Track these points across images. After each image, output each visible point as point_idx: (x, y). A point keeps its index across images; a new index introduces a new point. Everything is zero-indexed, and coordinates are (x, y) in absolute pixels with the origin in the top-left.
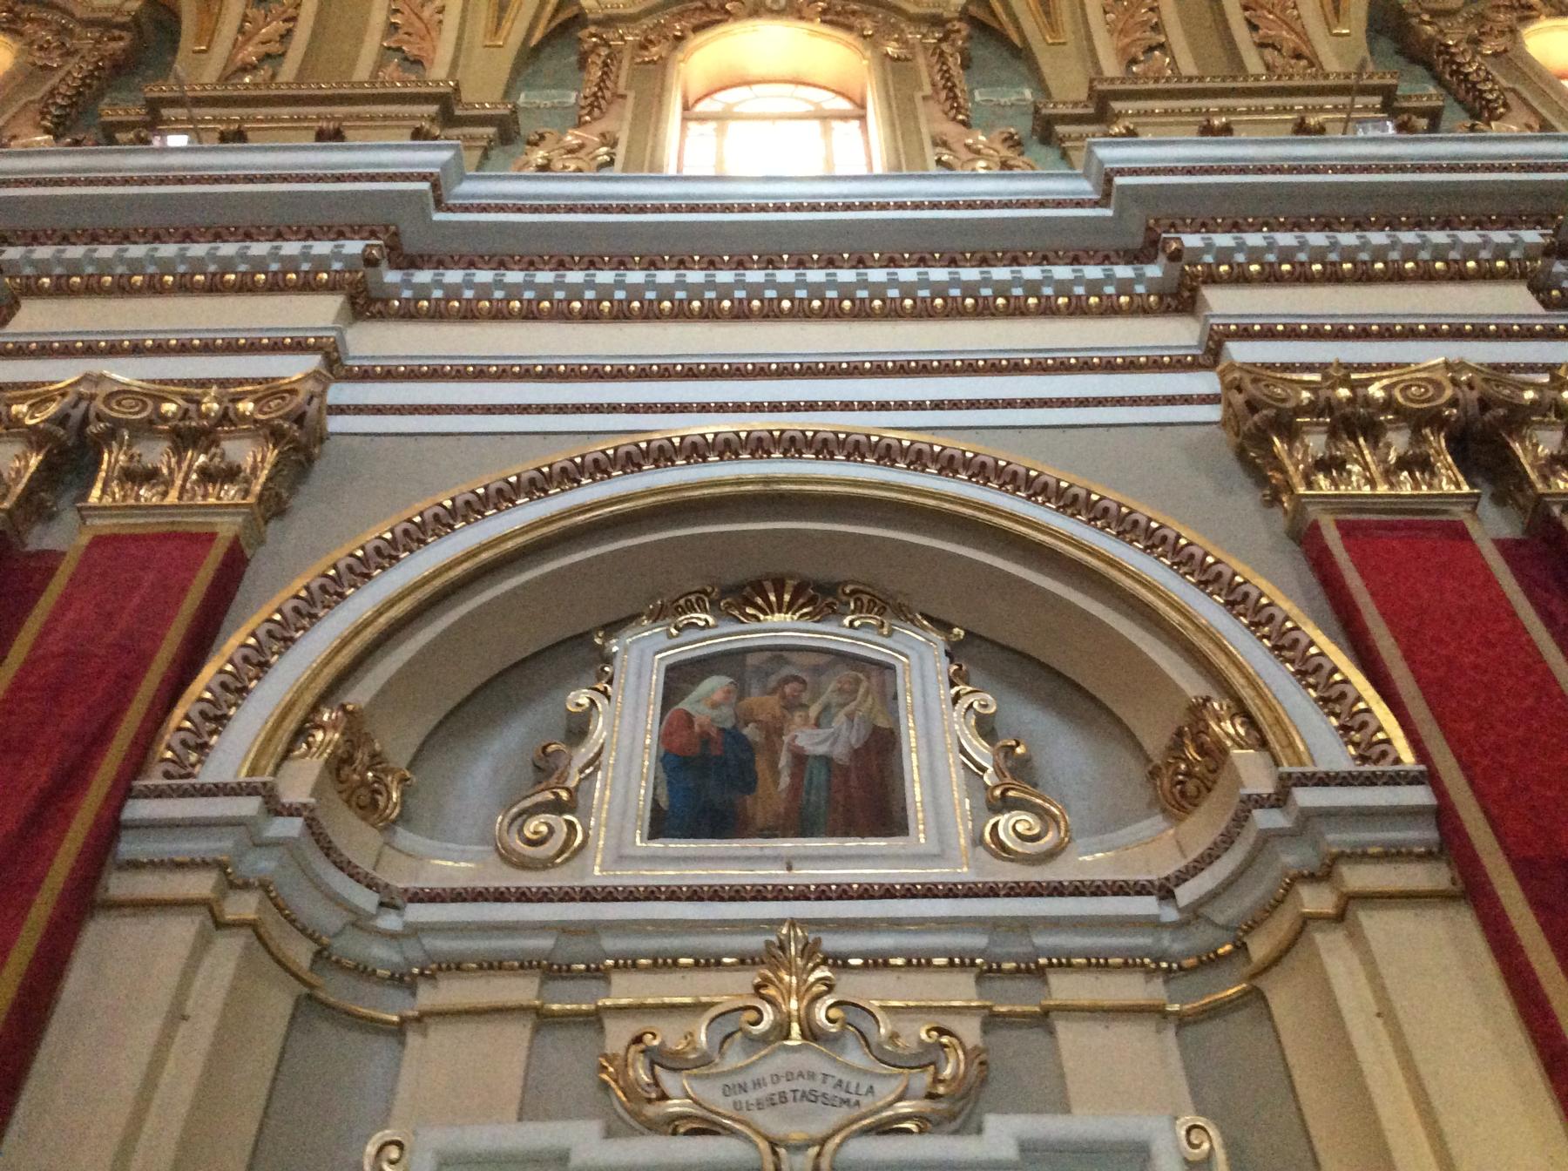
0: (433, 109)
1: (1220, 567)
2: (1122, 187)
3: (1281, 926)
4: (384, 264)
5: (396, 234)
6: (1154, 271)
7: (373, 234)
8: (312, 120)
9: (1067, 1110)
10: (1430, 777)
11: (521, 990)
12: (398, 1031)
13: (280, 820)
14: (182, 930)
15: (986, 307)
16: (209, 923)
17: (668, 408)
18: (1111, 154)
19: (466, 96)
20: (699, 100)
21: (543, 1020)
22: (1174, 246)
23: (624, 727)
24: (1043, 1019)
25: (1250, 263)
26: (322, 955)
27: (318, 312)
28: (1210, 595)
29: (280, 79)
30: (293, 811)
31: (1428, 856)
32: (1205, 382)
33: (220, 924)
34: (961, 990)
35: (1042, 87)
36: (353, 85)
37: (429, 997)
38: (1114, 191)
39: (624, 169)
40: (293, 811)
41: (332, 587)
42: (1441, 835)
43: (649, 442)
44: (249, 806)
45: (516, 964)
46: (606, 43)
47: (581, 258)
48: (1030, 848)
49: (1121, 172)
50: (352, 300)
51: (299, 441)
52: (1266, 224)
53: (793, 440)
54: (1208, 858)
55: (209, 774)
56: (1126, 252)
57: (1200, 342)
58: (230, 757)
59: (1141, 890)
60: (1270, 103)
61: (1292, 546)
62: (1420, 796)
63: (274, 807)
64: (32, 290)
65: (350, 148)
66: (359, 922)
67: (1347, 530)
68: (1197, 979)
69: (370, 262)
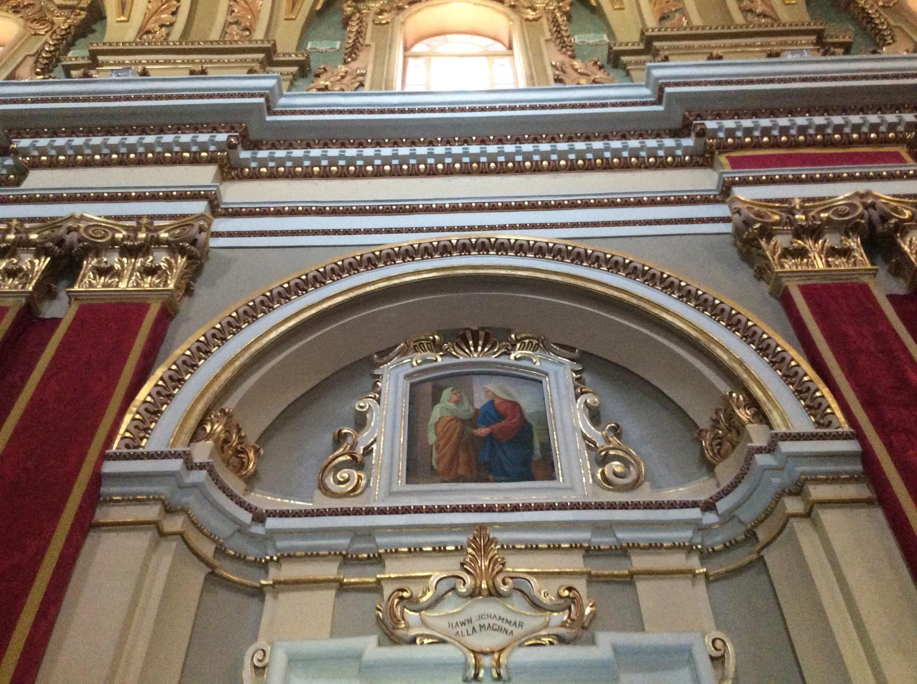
0: (261, 56)
1: (739, 316)
2: (670, 93)
3: (774, 523)
4: (239, 147)
5: (246, 129)
6: (688, 142)
7: (233, 129)
8: (773, 46)
9: (642, 629)
10: (858, 435)
11: (330, 570)
12: (259, 593)
13: (193, 472)
14: (141, 540)
15: (608, 163)
16: (157, 535)
17: (389, 231)
18: (660, 72)
19: (280, 49)
20: (412, 46)
21: (342, 588)
22: (699, 128)
23: (385, 416)
24: (629, 580)
25: (763, 137)
26: (220, 551)
27: (203, 176)
28: (734, 332)
29: (170, 39)
30: (201, 467)
31: (852, 479)
32: (722, 210)
33: (162, 534)
34: (576, 562)
35: (611, 35)
36: (104, 44)
37: (275, 573)
38: (665, 95)
39: (371, 88)
40: (201, 467)
41: (219, 335)
42: (864, 468)
43: (381, 251)
44: (176, 465)
45: (406, 550)
46: (359, 11)
47: (285, 141)
48: (628, 480)
49: (668, 85)
50: (221, 167)
51: (192, 250)
52: (808, 112)
53: (426, 248)
54: (733, 486)
55: (147, 445)
56: (670, 131)
57: (718, 187)
58: (160, 437)
59: (695, 505)
60: (179, 58)
61: (773, 301)
62: (852, 446)
63: (190, 466)
64: (36, 165)
65: (210, 79)
66: (242, 529)
67: (807, 291)
68: (723, 557)
69: (231, 146)
